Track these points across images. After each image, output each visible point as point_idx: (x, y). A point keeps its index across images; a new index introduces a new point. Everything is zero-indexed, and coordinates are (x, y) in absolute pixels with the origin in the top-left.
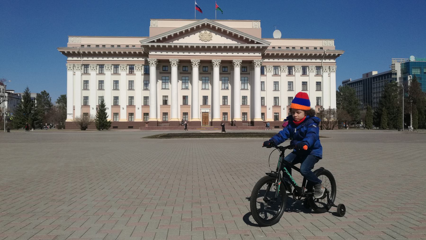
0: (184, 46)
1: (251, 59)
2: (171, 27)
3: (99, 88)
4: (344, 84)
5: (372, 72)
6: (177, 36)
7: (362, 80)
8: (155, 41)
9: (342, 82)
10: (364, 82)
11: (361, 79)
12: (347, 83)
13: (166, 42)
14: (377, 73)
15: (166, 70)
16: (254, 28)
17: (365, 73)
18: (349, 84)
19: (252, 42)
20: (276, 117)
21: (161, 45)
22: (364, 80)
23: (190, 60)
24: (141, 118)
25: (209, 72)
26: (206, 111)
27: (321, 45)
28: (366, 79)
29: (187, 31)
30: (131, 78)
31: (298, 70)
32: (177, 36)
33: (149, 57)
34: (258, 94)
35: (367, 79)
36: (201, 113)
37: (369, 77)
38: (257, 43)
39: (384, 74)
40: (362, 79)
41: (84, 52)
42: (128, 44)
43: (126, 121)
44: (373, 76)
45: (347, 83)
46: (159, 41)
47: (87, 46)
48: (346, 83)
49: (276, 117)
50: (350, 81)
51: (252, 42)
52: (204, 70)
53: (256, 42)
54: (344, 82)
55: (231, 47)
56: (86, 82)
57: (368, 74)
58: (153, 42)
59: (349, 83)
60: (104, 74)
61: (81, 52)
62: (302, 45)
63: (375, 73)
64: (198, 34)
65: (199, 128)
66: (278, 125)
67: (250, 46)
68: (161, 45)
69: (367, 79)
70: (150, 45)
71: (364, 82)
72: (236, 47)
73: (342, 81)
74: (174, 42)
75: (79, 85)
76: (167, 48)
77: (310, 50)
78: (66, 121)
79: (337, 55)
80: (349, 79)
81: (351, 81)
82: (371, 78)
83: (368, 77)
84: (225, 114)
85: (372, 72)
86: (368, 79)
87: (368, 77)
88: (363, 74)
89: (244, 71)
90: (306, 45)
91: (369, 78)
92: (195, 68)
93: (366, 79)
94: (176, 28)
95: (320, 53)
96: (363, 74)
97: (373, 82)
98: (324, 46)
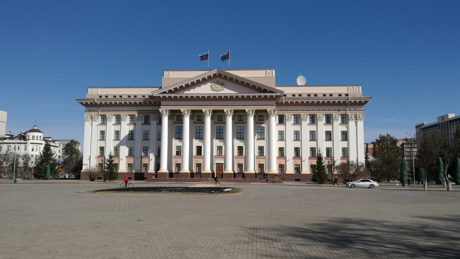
0: (201, 96)
1: (244, 109)
2: (183, 78)
3: (129, 139)
4: (418, 128)
5: (448, 114)
6: (188, 87)
7: (437, 124)
8: (167, 92)
9: (415, 126)
10: (439, 126)
11: (437, 122)
12: (421, 127)
13: (178, 93)
14: (454, 116)
15: (200, 120)
16: (268, 76)
17: (440, 116)
18: (423, 129)
19: (265, 91)
20: (298, 169)
21: (172, 95)
22: (439, 124)
23: (201, 110)
24: (153, 170)
25: (244, 121)
26: (220, 162)
27: (346, 92)
28: (441, 123)
29: (198, 81)
30: (146, 127)
31: (95, 120)
32: (188, 87)
33: (160, 108)
34: (275, 145)
35: (443, 123)
36: (215, 164)
37: (445, 120)
38: (270, 92)
39: (456, 119)
40: (437, 123)
41: (130, 103)
42: (295, 92)
43: (126, 171)
44: (450, 120)
45: (421, 127)
46: (170, 92)
47: (298, 95)
48: (420, 128)
49: (298, 169)
50: (424, 124)
51: (265, 91)
52: (239, 119)
53: (268, 91)
54: (417, 126)
55: (231, 97)
56: (103, 133)
57: (443, 117)
58: (165, 93)
59: (422, 127)
60: (149, 124)
61: (99, 103)
62: (309, 92)
63: (451, 116)
64: (209, 84)
65: (205, 181)
66: (299, 178)
67: (263, 95)
68: (172, 95)
69: (443, 123)
70: (161, 96)
71: (439, 126)
72: (237, 97)
73: (416, 125)
74: (185, 92)
75: (97, 135)
76: (195, 99)
77: (318, 98)
78: (82, 171)
79: (363, 102)
80: (423, 123)
81: (425, 124)
82: (447, 122)
83: (444, 121)
84: (240, 166)
85: (447, 115)
86: (446, 121)
87: (444, 120)
88: (438, 117)
89: (240, 120)
90: (293, 92)
91: (445, 122)
92: (208, 118)
93: (442, 123)
94: (188, 79)
95: (302, 101)
96: (438, 117)
97: (449, 127)
98: (349, 92)
